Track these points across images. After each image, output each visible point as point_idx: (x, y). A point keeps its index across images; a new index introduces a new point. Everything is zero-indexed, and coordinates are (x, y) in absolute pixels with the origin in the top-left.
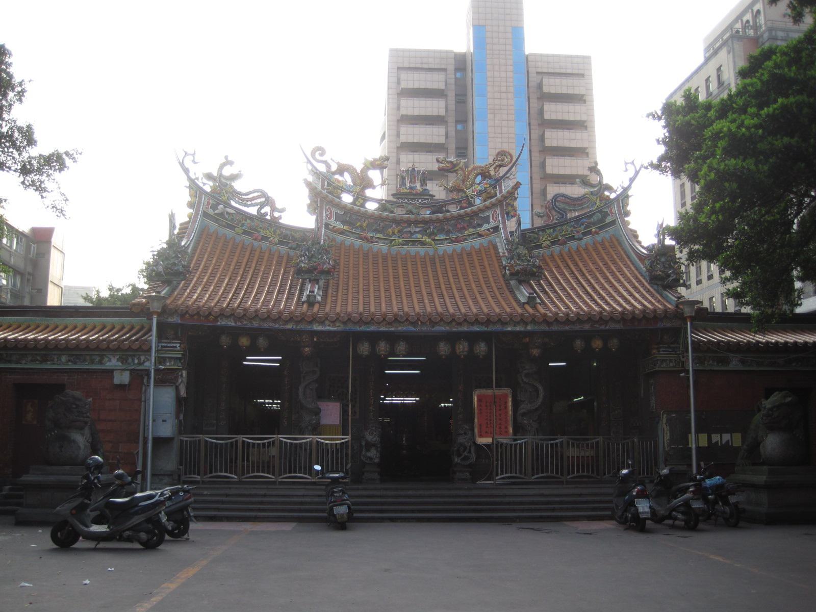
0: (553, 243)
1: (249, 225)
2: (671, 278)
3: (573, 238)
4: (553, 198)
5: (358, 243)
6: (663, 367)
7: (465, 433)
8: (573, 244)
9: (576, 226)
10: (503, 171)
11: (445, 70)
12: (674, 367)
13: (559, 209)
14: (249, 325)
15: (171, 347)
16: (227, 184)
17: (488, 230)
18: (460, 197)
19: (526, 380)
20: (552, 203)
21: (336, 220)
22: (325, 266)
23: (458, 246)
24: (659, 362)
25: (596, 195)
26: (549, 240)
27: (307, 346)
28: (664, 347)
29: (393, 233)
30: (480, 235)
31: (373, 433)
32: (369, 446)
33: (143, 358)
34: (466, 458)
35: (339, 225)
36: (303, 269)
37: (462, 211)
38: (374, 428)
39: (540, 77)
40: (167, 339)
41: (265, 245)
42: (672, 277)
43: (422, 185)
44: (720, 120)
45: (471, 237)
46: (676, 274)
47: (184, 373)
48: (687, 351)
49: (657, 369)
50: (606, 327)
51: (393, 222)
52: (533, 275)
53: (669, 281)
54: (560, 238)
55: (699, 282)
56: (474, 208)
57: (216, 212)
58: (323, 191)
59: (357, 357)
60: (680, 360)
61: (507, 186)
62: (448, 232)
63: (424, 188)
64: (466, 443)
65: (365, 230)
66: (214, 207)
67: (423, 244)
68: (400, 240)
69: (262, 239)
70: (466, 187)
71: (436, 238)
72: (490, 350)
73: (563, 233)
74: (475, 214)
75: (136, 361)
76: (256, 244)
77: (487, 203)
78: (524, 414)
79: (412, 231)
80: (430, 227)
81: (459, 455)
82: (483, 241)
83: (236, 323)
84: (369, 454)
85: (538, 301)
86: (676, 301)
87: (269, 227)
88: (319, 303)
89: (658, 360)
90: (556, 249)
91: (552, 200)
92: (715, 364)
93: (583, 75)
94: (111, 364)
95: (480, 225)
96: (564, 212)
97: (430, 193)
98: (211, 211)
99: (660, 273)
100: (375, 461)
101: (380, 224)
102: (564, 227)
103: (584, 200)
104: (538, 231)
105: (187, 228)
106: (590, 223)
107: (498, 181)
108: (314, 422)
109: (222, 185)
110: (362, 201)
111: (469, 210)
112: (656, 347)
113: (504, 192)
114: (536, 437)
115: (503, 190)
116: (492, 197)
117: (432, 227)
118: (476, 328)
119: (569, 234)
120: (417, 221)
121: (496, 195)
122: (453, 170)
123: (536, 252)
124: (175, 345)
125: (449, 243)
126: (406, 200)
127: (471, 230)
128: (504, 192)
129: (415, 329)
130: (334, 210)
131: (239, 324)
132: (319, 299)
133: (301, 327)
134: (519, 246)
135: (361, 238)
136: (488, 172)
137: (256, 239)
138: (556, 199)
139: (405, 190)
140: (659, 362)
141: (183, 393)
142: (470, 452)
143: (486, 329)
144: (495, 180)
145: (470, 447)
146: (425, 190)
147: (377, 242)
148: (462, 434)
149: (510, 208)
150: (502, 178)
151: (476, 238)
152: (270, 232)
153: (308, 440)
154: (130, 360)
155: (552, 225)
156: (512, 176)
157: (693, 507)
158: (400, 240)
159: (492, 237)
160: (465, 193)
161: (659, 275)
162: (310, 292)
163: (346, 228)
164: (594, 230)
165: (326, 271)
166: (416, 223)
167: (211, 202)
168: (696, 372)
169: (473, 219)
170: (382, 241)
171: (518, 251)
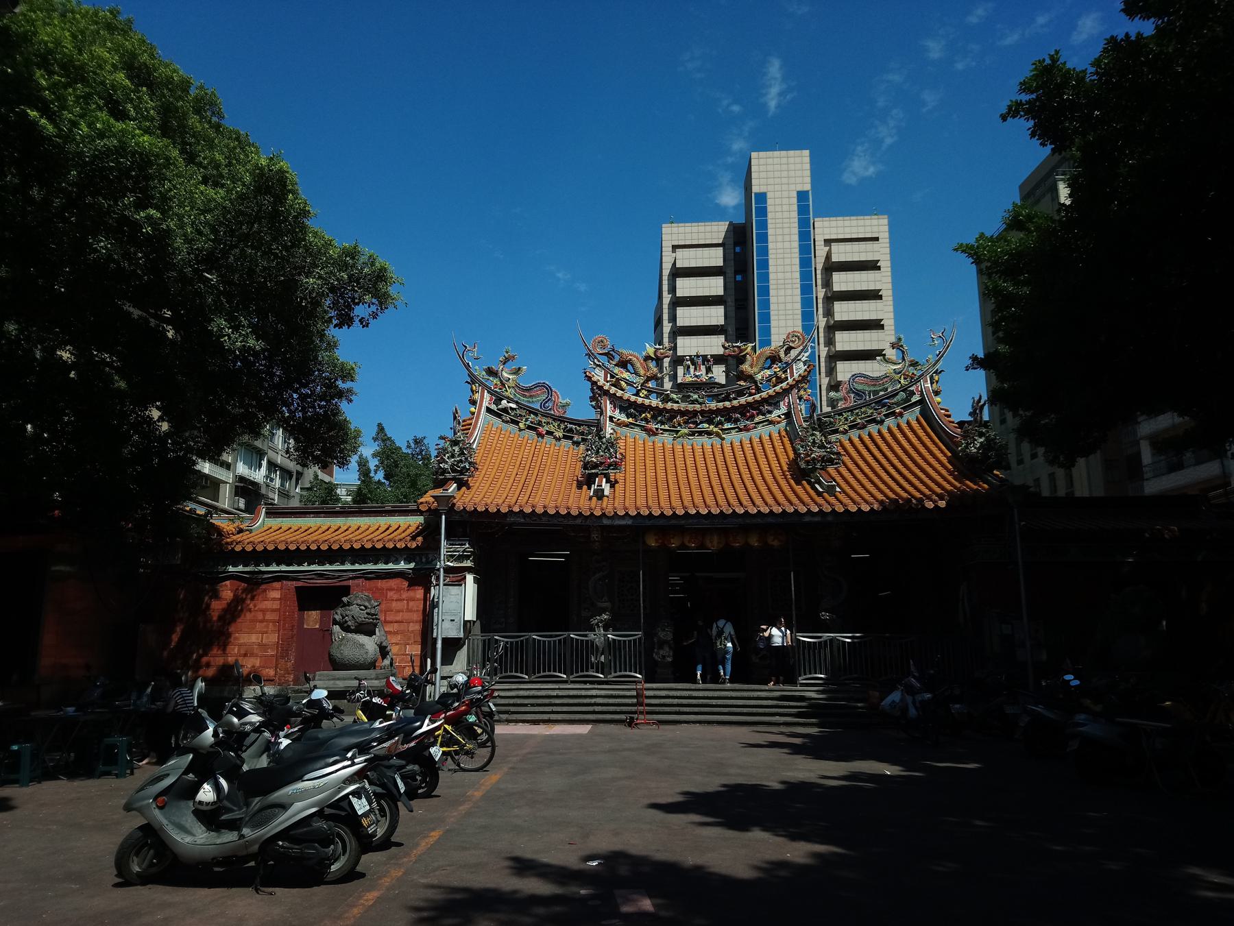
0: (851, 427)
3: (874, 421)
13: (857, 390)
16: (509, 379)
17: (779, 416)
26: (847, 424)
29: (679, 425)
30: (771, 422)
33: (431, 557)
35: (623, 418)
43: (707, 373)
45: (761, 425)
52: (831, 462)
54: (859, 421)
55: (1020, 462)
56: (764, 395)
57: (500, 407)
62: (736, 421)
63: (710, 375)
65: (650, 422)
67: (709, 433)
69: (546, 434)
75: (424, 560)
83: (525, 519)
85: (838, 489)
88: (608, 497)
90: (854, 435)
91: (849, 381)
93: (877, 239)
95: (770, 412)
96: (863, 393)
97: (716, 381)
98: (493, 407)
105: (471, 424)
106: (893, 404)
107: (788, 365)
110: (646, 393)
111: (757, 397)
115: (795, 374)
123: (833, 438)
126: (692, 390)
128: (796, 376)
132: (607, 492)
143: (782, 520)
144: (786, 363)
146: (711, 378)
147: (662, 434)
150: (793, 360)
152: (554, 426)
153: (638, 636)
155: (848, 408)
157: (1007, 712)
158: (686, 431)
162: (598, 486)
163: (630, 420)
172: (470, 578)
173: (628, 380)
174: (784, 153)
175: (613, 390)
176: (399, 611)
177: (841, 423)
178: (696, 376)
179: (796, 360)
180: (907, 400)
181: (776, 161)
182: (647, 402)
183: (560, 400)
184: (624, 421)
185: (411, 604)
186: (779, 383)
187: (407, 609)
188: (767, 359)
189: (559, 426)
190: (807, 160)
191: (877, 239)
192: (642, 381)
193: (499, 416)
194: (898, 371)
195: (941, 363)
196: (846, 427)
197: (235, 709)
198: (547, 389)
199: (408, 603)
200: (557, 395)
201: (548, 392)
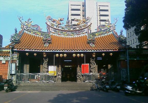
5: (57, 35)
6: (122, 59)
8: (103, 35)
11: (80, 5)
14: (32, 51)
23: (79, 36)
32: (59, 75)
35: (54, 32)
37: (79, 29)
39: (99, 6)
41: (38, 36)
44: (61, 79)
47: (18, 61)
61: (89, 24)
67: (71, 35)
72: (84, 55)
74: (82, 29)
75: (7, 58)
76: (36, 35)
77: (85, 27)
78: (92, 69)
82: (84, 35)
84: (59, 77)
90: (99, 36)
98: (26, 29)
118: (81, 51)
130: (52, 29)
131: (30, 50)
133: (44, 51)
141: (18, 65)
149: (89, 28)
154: (6, 58)
159: (86, 34)
166: (70, 31)
167: (26, 27)
169: (81, 30)
182: (58, 29)
188: (83, 22)
193: (27, 31)
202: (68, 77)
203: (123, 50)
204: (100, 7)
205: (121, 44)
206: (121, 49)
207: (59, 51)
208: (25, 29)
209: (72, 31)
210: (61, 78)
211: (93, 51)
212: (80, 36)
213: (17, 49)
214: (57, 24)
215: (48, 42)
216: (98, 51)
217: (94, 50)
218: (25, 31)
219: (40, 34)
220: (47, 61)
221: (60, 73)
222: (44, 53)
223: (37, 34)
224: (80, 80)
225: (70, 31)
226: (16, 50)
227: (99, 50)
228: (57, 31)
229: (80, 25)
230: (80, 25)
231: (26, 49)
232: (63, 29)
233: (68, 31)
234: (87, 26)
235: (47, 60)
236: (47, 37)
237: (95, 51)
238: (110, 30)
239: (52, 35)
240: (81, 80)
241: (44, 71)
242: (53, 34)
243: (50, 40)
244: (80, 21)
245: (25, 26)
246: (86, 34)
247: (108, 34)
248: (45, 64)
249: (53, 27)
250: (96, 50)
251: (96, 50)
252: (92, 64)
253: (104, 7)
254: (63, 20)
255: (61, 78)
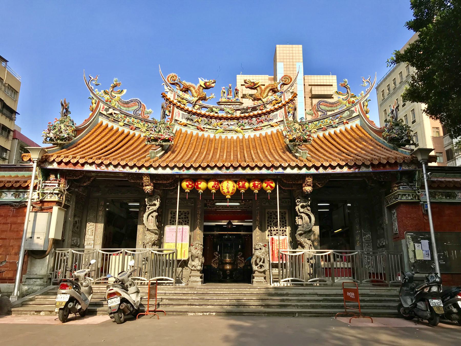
1: (128, 121)
2: (404, 139)
3: (332, 126)
4: (318, 103)
5: (195, 132)
6: (404, 199)
7: (260, 249)
8: (332, 131)
9: (333, 119)
10: (285, 87)
12: (411, 199)
13: (322, 109)
15: (51, 186)
16: (115, 96)
17: (276, 123)
18: (259, 103)
19: (302, 210)
20: (317, 105)
21: (182, 118)
22: (166, 136)
23: (257, 133)
24: (400, 196)
25: (345, 100)
27: (148, 186)
28: (404, 185)
30: (272, 126)
31: (196, 248)
34: (261, 266)
35: (184, 121)
36: (152, 138)
38: (197, 245)
39: (310, 87)
40: (50, 180)
42: (405, 138)
44: (201, 272)
45: (266, 127)
46: (408, 136)
48: (423, 187)
49: (399, 201)
50: (359, 170)
51: (217, 119)
52: (306, 141)
53: (402, 141)
56: (268, 110)
58: (174, 100)
59: (182, 190)
60: (416, 194)
61: (288, 96)
63: (237, 98)
64: (261, 256)
66: (107, 110)
68: (222, 130)
70: (263, 97)
71: (244, 128)
73: (325, 124)
74: (269, 113)
76: (132, 132)
78: (301, 235)
79: (229, 124)
80: (240, 122)
81: (257, 264)
82: (274, 130)
83: (96, 168)
84: (193, 263)
86: (411, 152)
87: (141, 122)
89: (399, 195)
91: (317, 104)
92: (444, 197)
93: (332, 85)
94: (7, 198)
98: (104, 113)
99: (396, 136)
100: (198, 268)
101: (209, 120)
102: (325, 120)
103: (338, 104)
104: (309, 123)
108: (153, 239)
109: (112, 97)
110: (198, 107)
111: (264, 111)
112: (397, 185)
113: (287, 100)
114: (311, 250)
116: (279, 103)
117: (241, 121)
118: (264, 171)
119: (329, 124)
120: (232, 118)
121: (281, 102)
122: (254, 87)
124: (54, 184)
125: (252, 131)
127: (266, 123)
129: (222, 172)
130: (181, 112)
133: (143, 171)
134: (295, 123)
135: (198, 129)
136: (277, 88)
137: (131, 129)
138: (319, 103)
139: (225, 100)
140: (400, 196)
142: (264, 262)
145: (264, 259)
146: (237, 99)
147: (207, 131)
148: (258, 249)
150: (285, 91)
151: (269, 128)
152: (141, 125)
156: (291, 90)
160: (262, 101)
161: (395, 137)
163: (188, 122)
164: (345, 121)
165: (167, 140)
167: (106, 107)
168: (431, 203)
170: (211, 130)
171: (294, 126)
172: (56, 209)
173: (188, 99)
174: (291, 46)
175: (179, 104)
176: (3, 231)
177: (312, 128)
178: (229, 98)
179: (287, 91)
180: (350, 115)
181: (287, 49)
182: (198, 112)
183: (146, 110)
184: (184, 123)
185: (13, 226)
186: (277, 103)
187: (10, 229)
188: (271, 90)
189: (144, 125)
190: (301, 49)
191: (332, 85)
192: (196, 100)
194: (344, 99)
195: (368, 95)
196: (315, 129)
197: (445, 244)
198: (138, 103)
199: (11, 226)
200: (144, 107)
201: (139, 105)
202: (228, 267)
203: (405, 168)
204: (313, 88)
205: (397, 151)
206: (401, 165)
207: (192, 171)
208: (101, 114)
209: (238, 119)
210: (199, 268)
211: (304, 171)
212: (263, 132)
213: (59, 163)
214: (195, 99)
215: (162, 146)
216: (321, 171)
217: (309, 168)
218: (101, 119)
219: (144, 130)
220: (155, 208)
221: (199, 252)
222: (146, 180)
223: (137, 128)
224: (263, 274)
225: (232, 119)
226: (55, 166)
227: (325, 168)
228: (195, 118)
229: (260, 99)
230: (260, 99)
231: (86, 163)
232: (212, 114)
233: (227, 119)
234: (283, 102)
235: (155, 205)
236: (160, 131)
237: (313, 171)
238: (354, 115)
239: (181, 130)
240: (265, 278)
241: (146, 242)
242: (184, 129)
243: (168, 140)
244: (261, 88)
245: (101, 105)
246: (281, 127)
247: (348, 126)
248: (150, 217)
249: (182, 106)
250: (314, 166)
251: (314, 166)
252: (302, 218)
253: (322, 88)
254: (213, 85)
255: (199, 268)
